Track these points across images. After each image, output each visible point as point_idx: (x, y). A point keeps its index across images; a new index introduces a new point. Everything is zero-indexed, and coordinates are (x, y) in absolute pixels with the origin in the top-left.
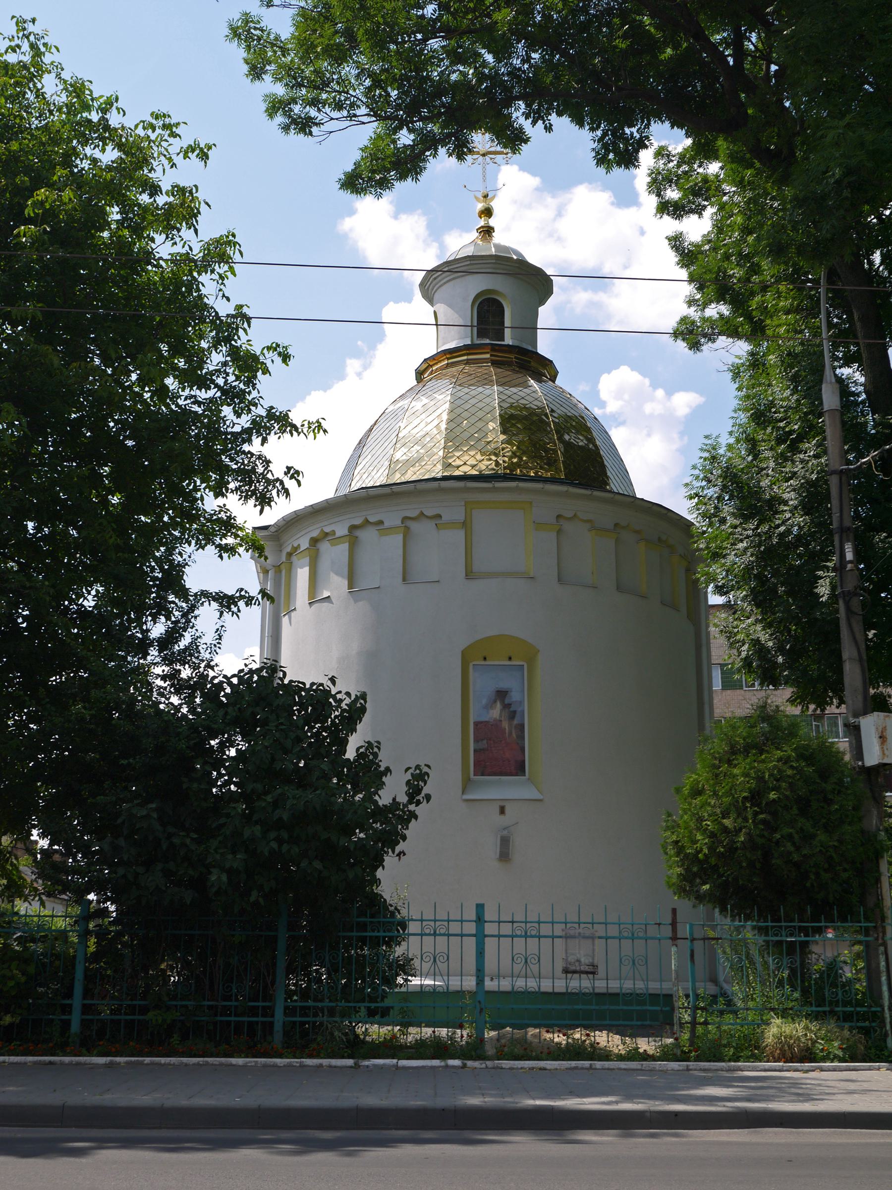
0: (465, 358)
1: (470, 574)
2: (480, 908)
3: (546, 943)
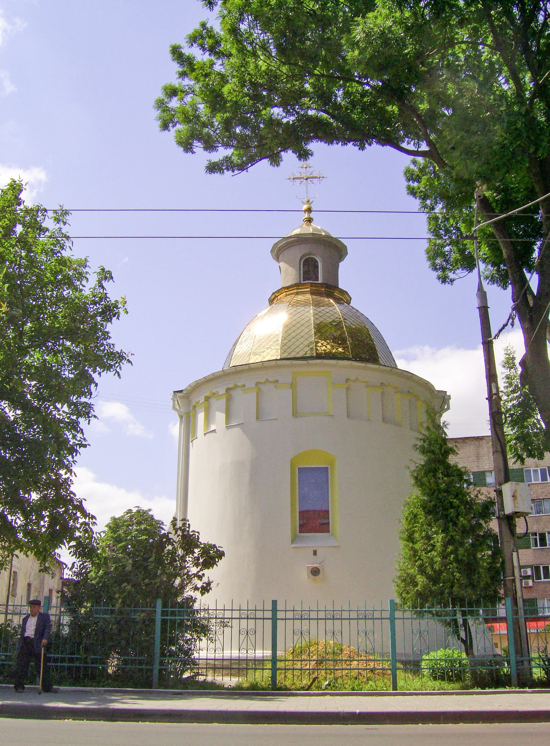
0: (296, 291)
1: (295, 414)
2: (274, 603)
3: (346, 622)
